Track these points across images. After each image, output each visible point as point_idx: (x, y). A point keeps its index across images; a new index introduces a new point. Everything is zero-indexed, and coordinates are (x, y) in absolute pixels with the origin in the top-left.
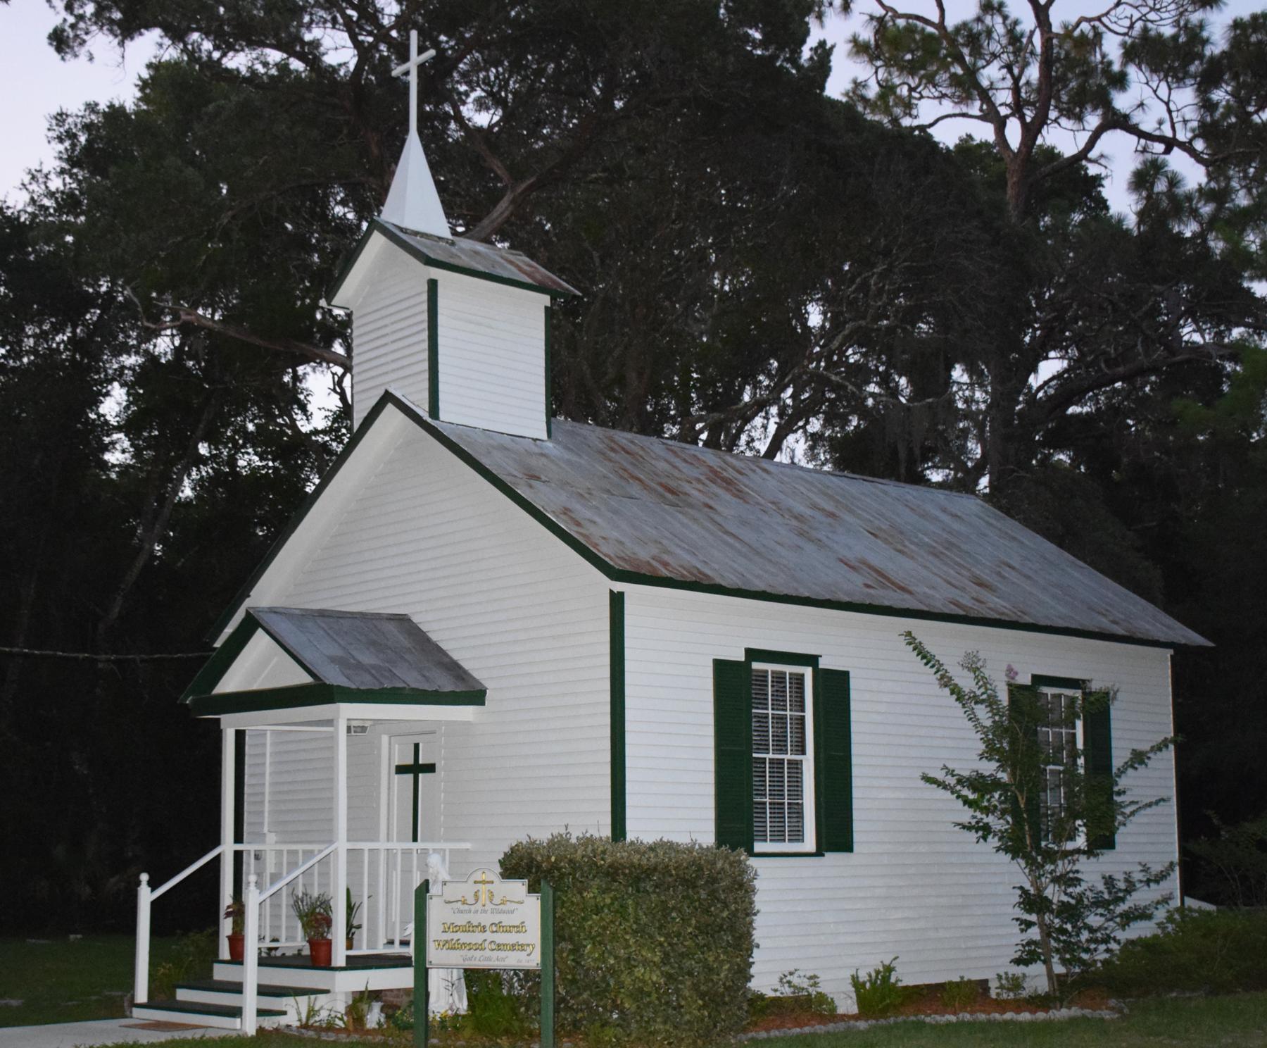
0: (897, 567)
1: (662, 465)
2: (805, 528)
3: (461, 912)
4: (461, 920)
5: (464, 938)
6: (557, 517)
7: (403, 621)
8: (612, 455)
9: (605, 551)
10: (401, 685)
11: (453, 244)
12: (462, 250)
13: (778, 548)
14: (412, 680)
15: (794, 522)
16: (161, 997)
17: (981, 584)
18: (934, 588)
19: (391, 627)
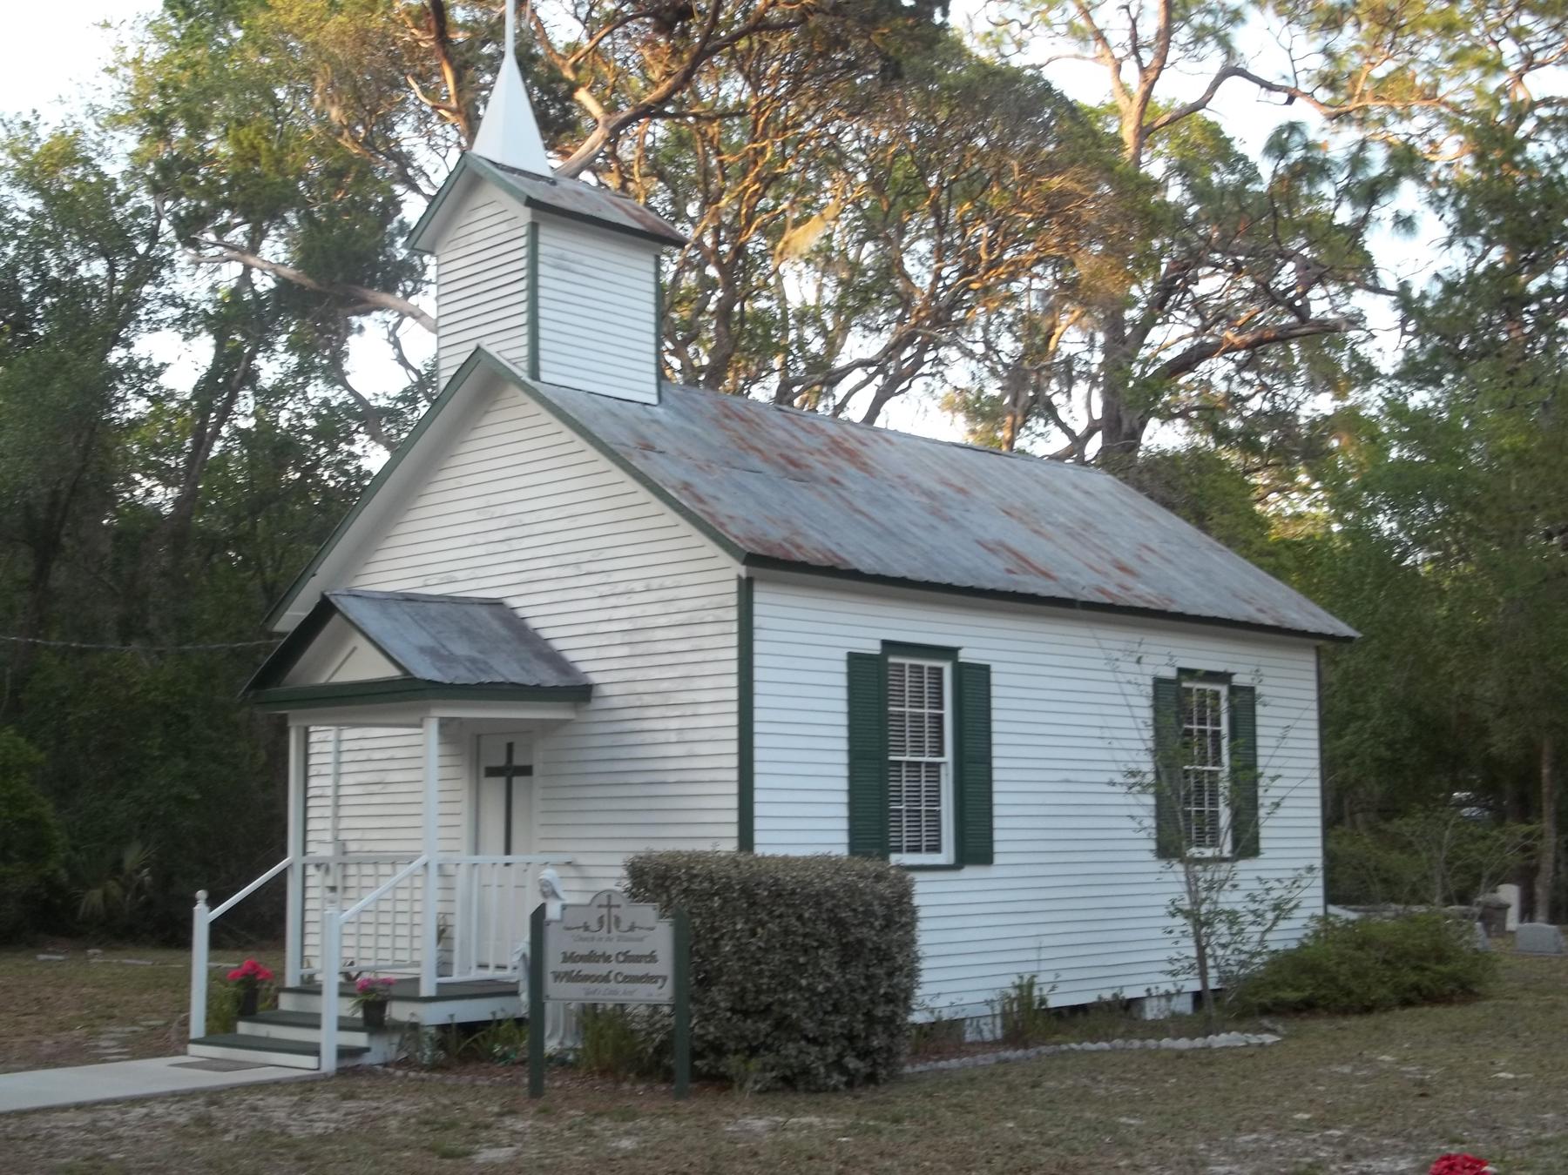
1: (780, 434)
2: (936, 504)
4: (583, 949)
7: (496, 604)
8: (727, 421)
9: (733, 530)
10: (499, 679)
13: (914, 530)
15: (924, 499)
16: (220, 1029)
18: (1075, 573)
19: (484, 612)
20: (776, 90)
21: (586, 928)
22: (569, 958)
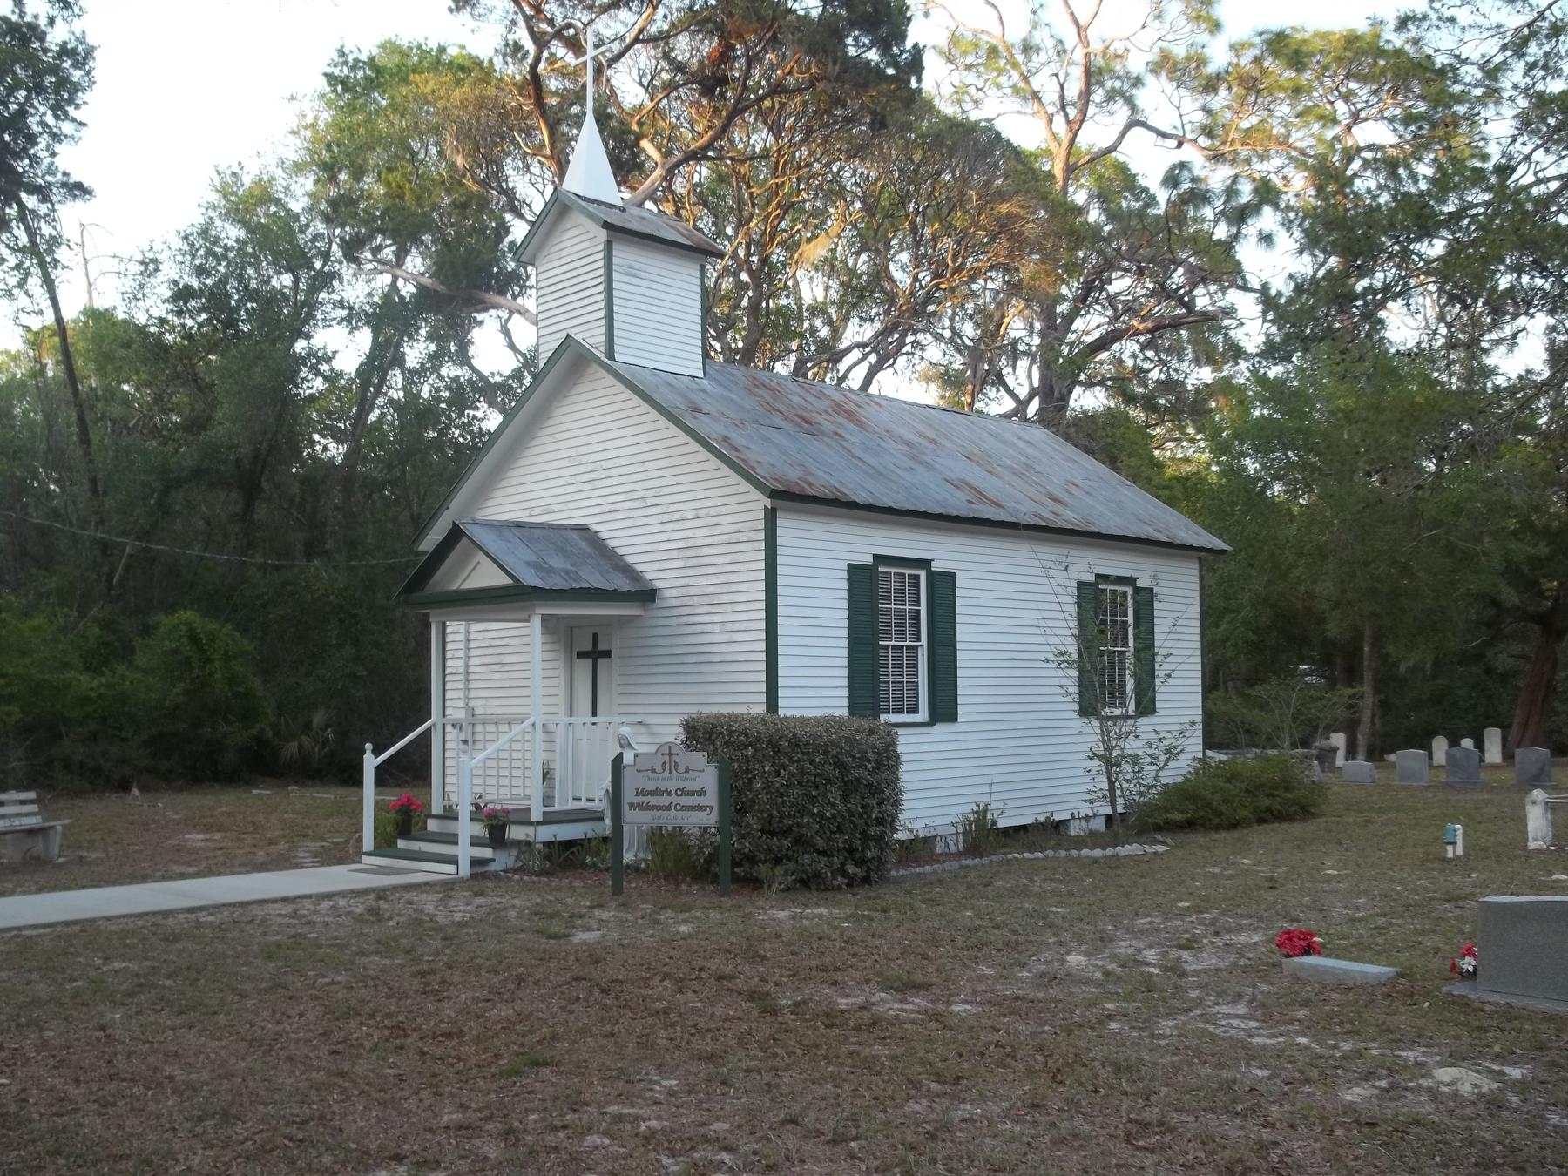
0: (992, 486)
2: (915, 452)
3: (651, 779)
4: (651, 786)
5: (653, 800)
6: (719, 444)
7: (583, 529)
9: (761, 472)
10: (587, 586)
11: (624, 210)
12: (632, 216)
13: (897, 470)
14: (597, 581)
15: (905, 448)
16: (385, 845)
17: (1055, 500)
19: (574, 535)
21: (653, 770)
22: (639, 793)
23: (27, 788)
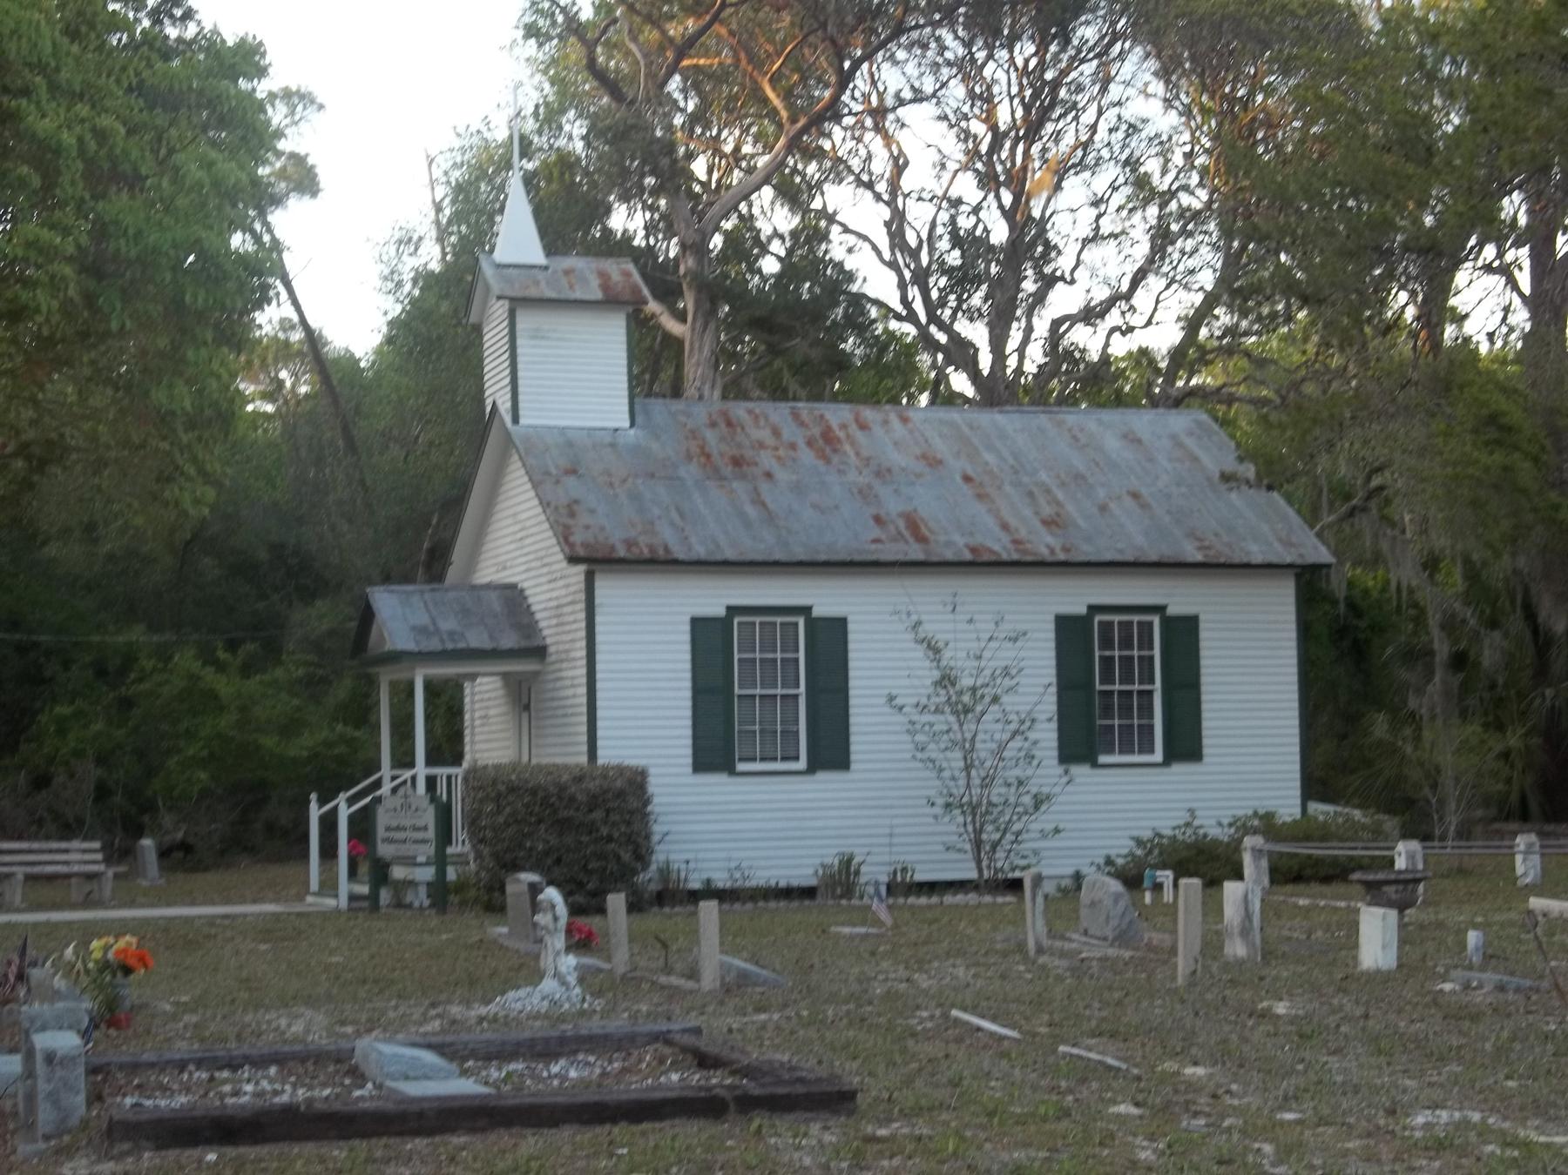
4: (394, 824)
20: (1042, 102)
22: (388, 829)
23: (92, 839)
